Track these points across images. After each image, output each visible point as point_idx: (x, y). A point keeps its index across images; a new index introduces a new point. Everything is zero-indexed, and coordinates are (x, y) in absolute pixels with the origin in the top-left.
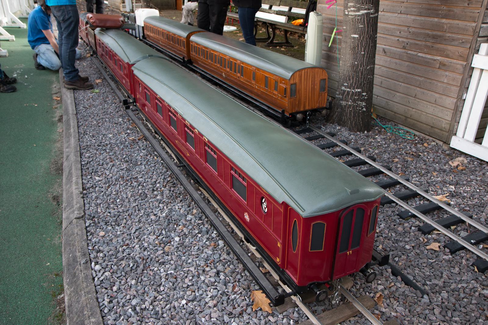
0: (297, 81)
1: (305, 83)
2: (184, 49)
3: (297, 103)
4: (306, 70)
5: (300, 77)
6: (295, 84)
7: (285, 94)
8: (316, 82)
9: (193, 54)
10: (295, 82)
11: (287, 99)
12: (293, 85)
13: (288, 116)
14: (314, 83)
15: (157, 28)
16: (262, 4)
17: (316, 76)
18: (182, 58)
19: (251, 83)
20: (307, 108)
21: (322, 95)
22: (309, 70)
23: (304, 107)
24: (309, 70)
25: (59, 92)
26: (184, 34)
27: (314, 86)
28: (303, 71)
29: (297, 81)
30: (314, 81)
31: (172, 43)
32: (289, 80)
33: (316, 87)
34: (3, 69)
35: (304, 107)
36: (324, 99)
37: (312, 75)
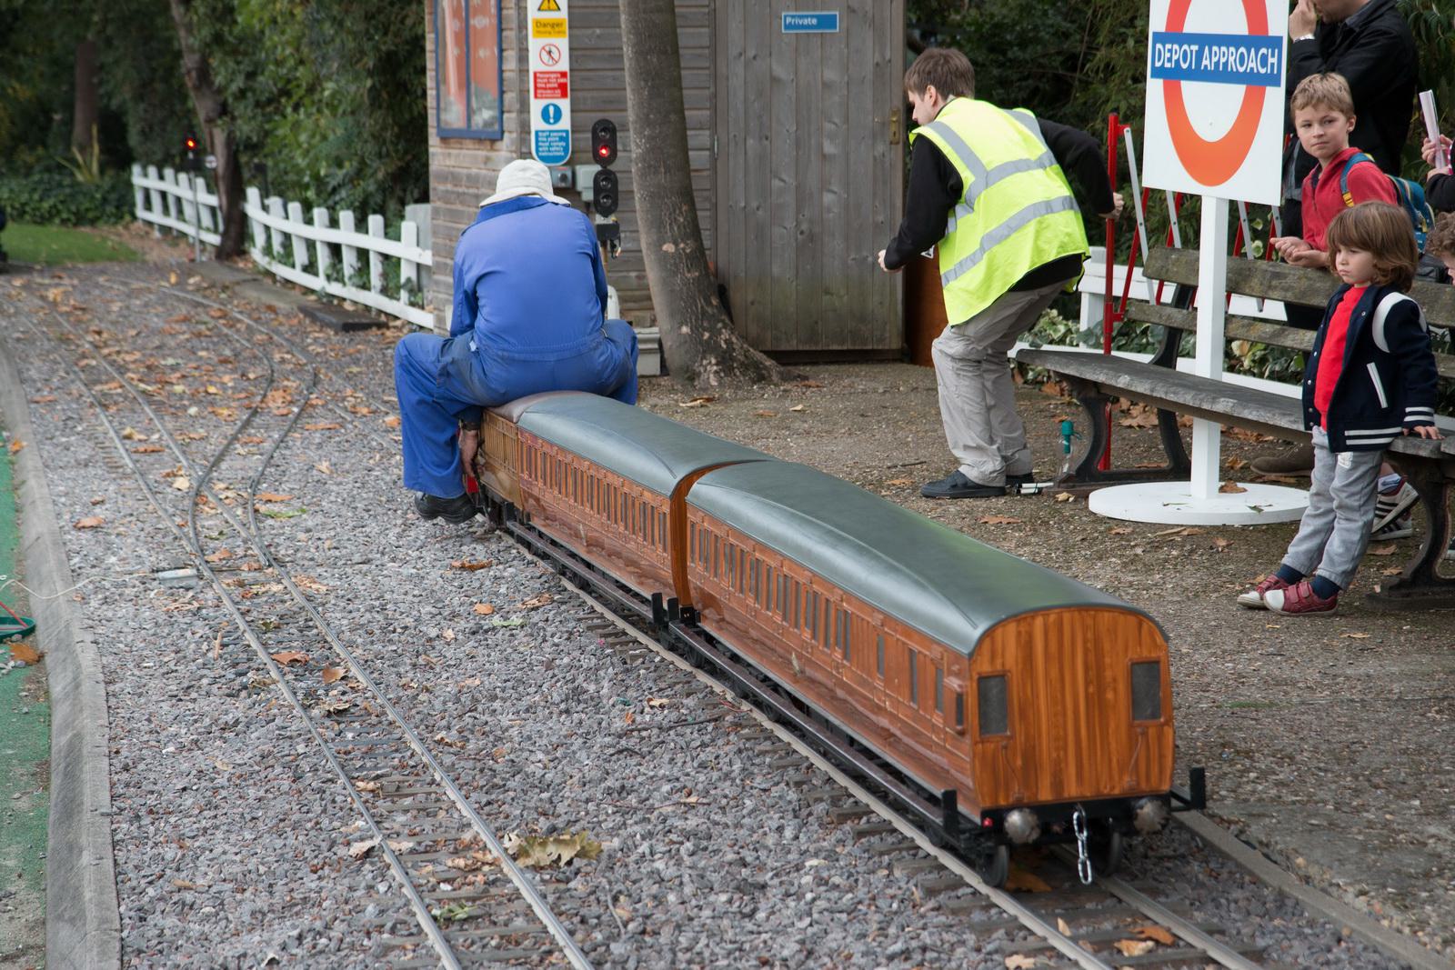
0: (1011, 657)
1: (1054, 673)
2: (659, 557)
3: (1019, 762)
4: (1052, 618)
5: (1027, 646)
6: (1002, 676)
7: (960, 721)
8: (1108, 674)
9: (697, 572)
10: (999, 667)
11: (967, 740)
12: (993, 682)
13: (977, 820)
14: (1100, 676)
15: (569, 459)
16: (1300, 397)
17: (1107, 646)
18: (938, 792)
19: (873, 689)
20: (1072, 790)
21: (1145, 734)
22: (1067, 616)
23: (1058, 784)
24: (1067, 616)
25: (28, 948)
26: (666, 477)
27: (1101, 690)
28: (1039, 621)
29: (1011, 657)
30: (1100, 668)
31: (778, 619)
32: (971, 655)
33: (1110, 695)
34: (5, 248)
35: (1058, 784)
36: (1161, 756)
37: (1085, 641)
